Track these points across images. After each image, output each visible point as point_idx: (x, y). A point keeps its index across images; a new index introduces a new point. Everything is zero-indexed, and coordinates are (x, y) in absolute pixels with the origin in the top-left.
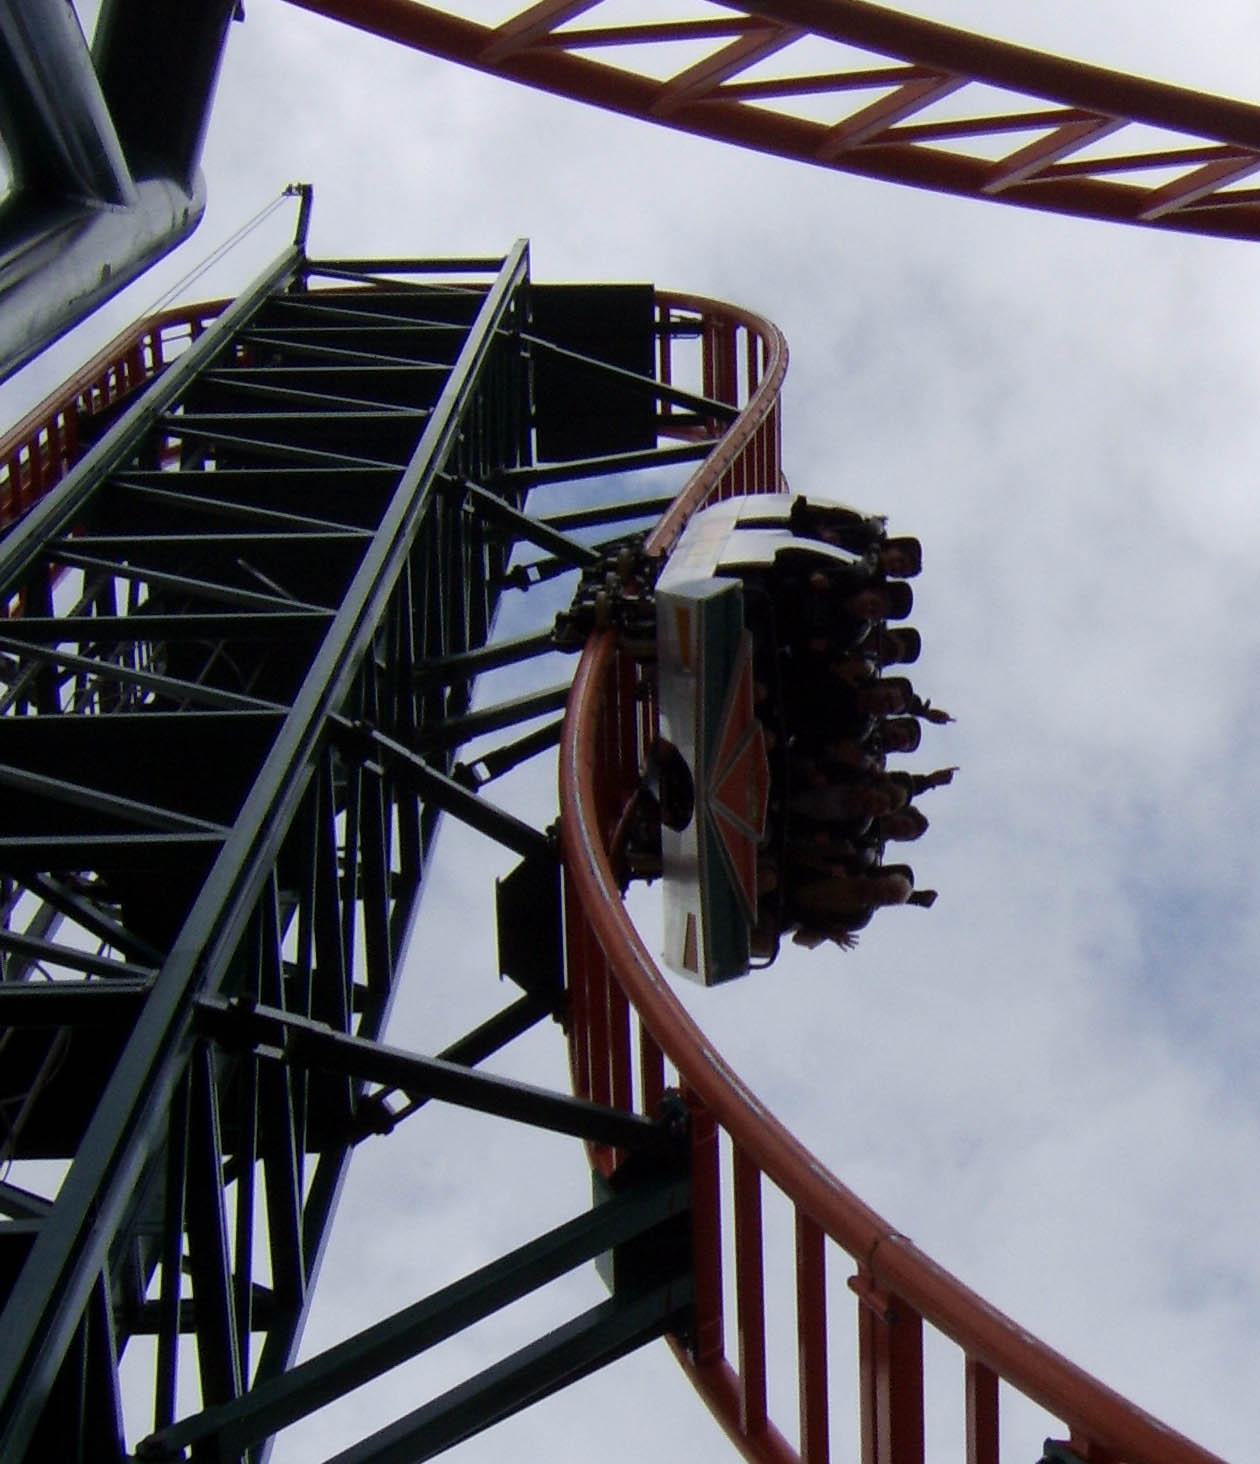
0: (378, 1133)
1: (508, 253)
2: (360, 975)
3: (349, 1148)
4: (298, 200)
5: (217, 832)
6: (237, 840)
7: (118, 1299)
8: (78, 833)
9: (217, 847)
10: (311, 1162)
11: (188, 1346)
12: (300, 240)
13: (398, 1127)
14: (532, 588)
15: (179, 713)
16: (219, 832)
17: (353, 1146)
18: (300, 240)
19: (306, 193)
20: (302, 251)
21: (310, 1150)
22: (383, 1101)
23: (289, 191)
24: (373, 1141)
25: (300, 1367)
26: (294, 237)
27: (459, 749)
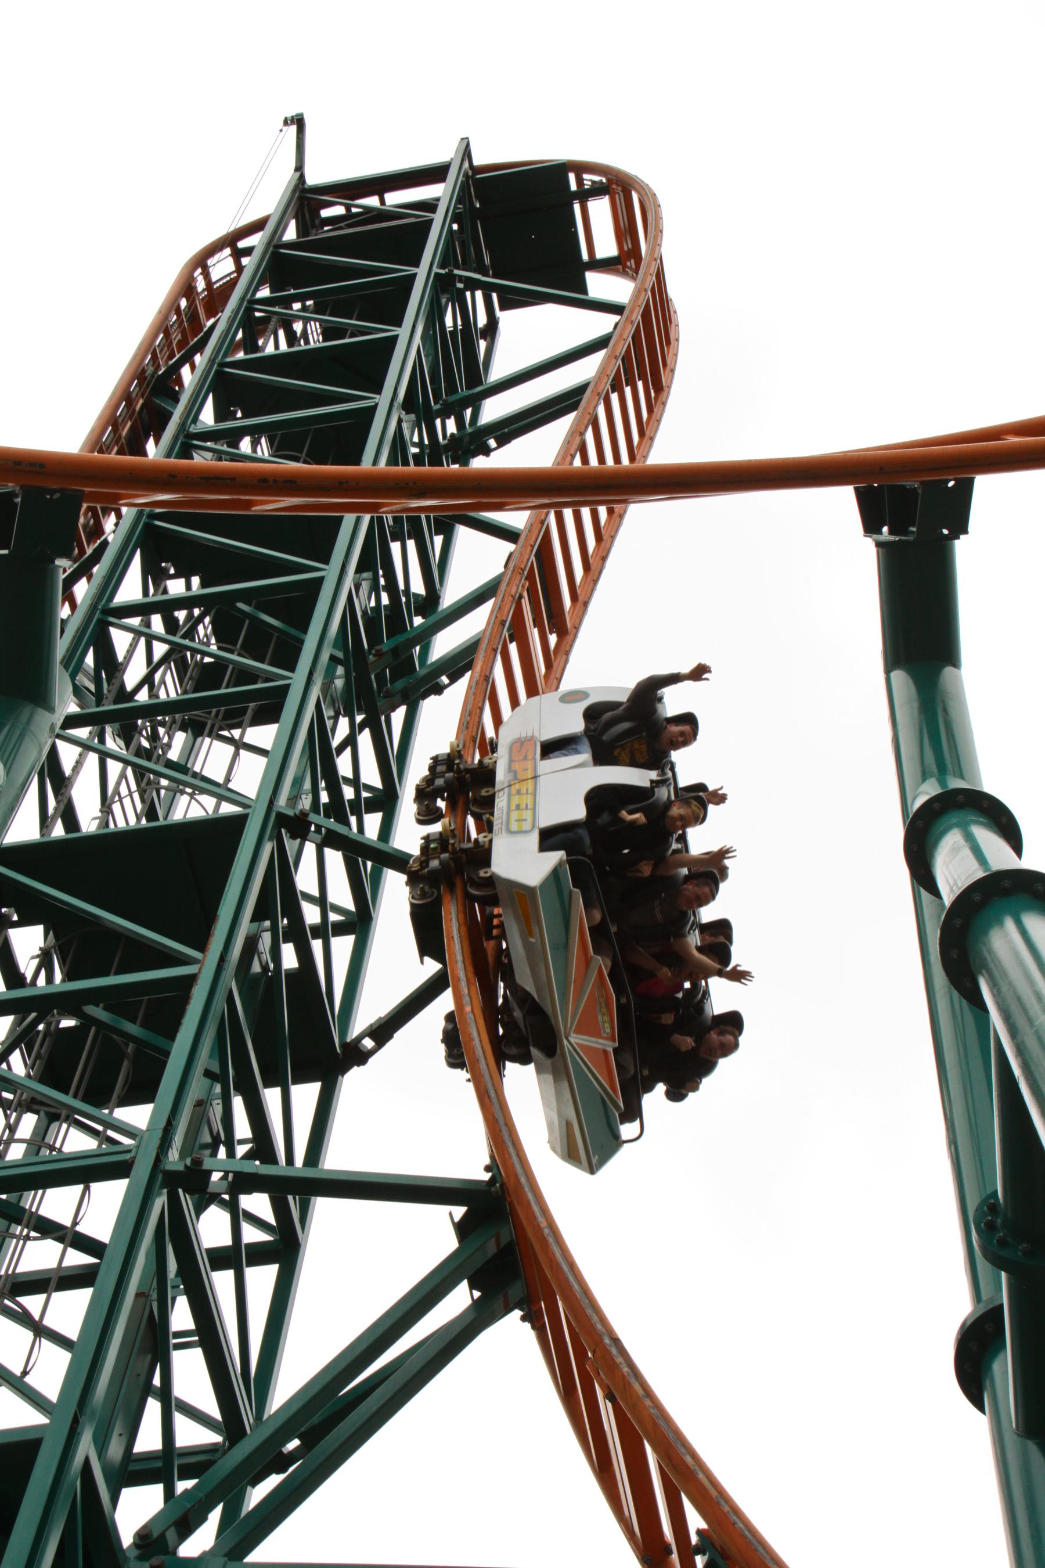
0: (359, 1065)
1: (453, 157)
2: (482, 320)
3: (340, 1077)
4: (294, 128)
5: (395, 331)
6: (421, 272)
7: (361, 614)
8: (85, 1045)
9: (415, 275)
10: (438, 540)
11: (411, 544)
12: (299, 168)
13: (446, 691)
14: (492, 454)
15: (223, 691)
16: (414, 270)
17: (343, 1076)
18: (299, 168)
19: (299, 122)
20: (302, 179)
21: (437, 534)
22: (488, 442)
23: (286, 122)
24: (433, 699)
25: (446, 608)
26: (293, 165)
27: (434, 637)
